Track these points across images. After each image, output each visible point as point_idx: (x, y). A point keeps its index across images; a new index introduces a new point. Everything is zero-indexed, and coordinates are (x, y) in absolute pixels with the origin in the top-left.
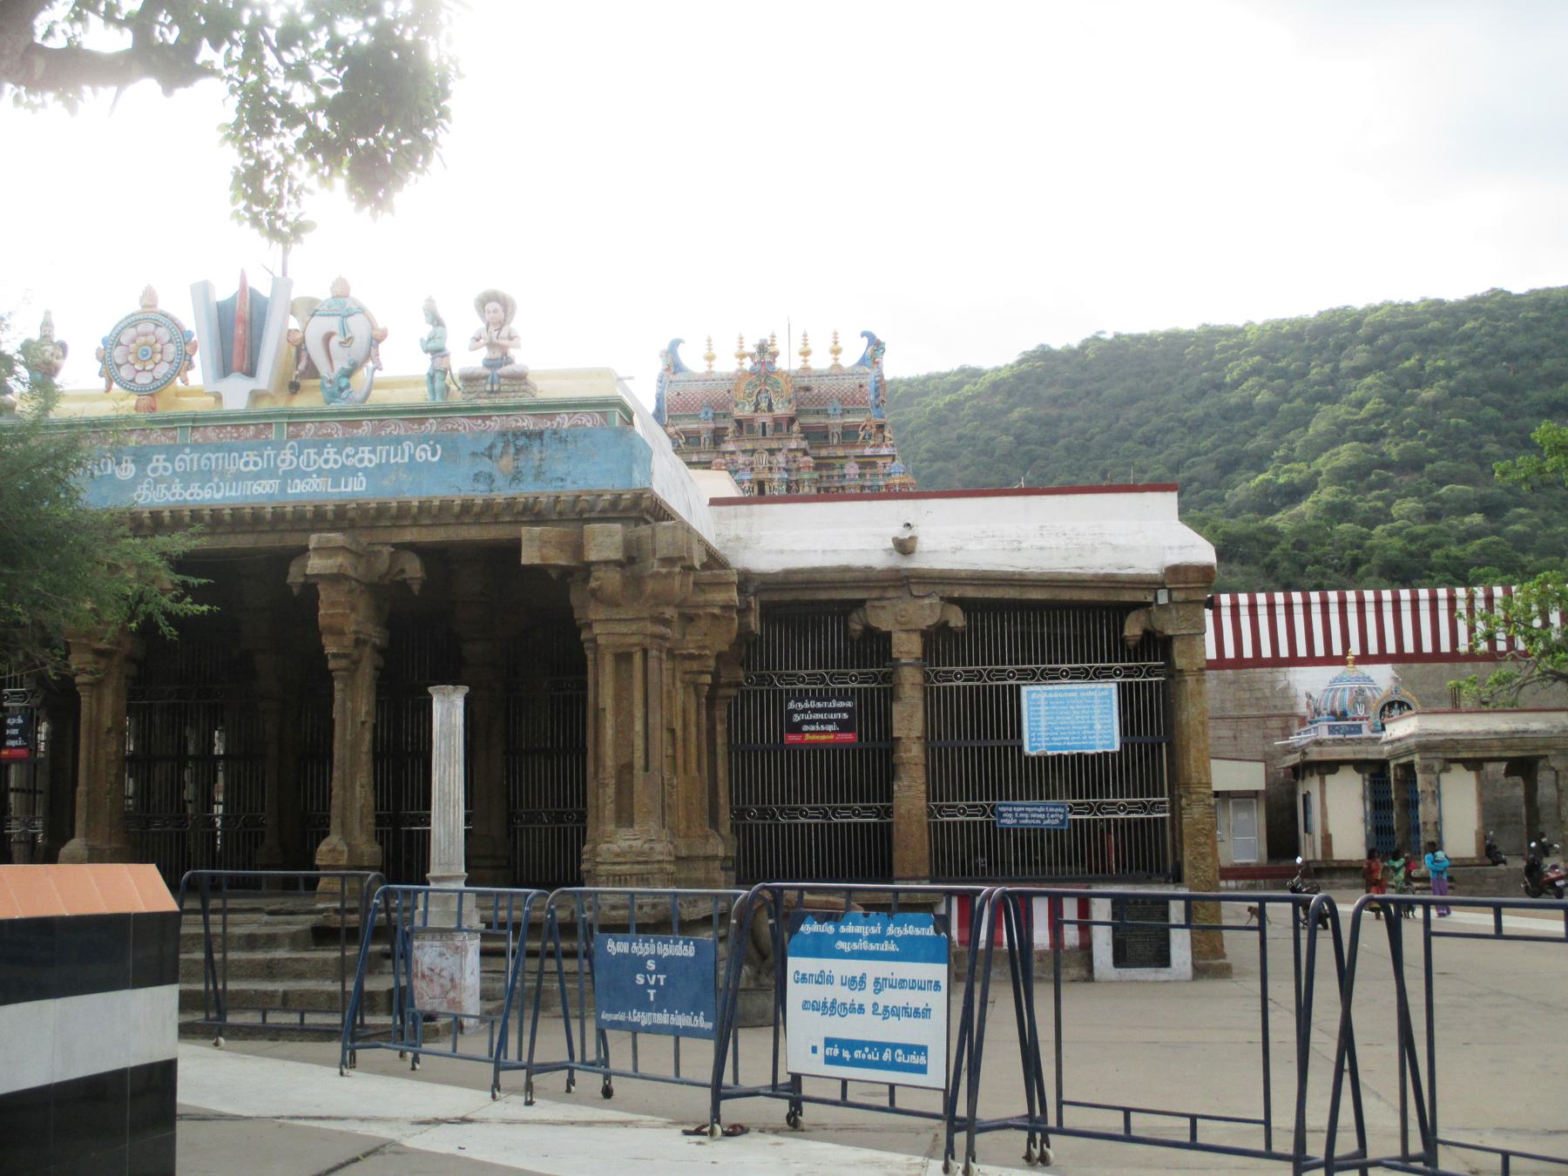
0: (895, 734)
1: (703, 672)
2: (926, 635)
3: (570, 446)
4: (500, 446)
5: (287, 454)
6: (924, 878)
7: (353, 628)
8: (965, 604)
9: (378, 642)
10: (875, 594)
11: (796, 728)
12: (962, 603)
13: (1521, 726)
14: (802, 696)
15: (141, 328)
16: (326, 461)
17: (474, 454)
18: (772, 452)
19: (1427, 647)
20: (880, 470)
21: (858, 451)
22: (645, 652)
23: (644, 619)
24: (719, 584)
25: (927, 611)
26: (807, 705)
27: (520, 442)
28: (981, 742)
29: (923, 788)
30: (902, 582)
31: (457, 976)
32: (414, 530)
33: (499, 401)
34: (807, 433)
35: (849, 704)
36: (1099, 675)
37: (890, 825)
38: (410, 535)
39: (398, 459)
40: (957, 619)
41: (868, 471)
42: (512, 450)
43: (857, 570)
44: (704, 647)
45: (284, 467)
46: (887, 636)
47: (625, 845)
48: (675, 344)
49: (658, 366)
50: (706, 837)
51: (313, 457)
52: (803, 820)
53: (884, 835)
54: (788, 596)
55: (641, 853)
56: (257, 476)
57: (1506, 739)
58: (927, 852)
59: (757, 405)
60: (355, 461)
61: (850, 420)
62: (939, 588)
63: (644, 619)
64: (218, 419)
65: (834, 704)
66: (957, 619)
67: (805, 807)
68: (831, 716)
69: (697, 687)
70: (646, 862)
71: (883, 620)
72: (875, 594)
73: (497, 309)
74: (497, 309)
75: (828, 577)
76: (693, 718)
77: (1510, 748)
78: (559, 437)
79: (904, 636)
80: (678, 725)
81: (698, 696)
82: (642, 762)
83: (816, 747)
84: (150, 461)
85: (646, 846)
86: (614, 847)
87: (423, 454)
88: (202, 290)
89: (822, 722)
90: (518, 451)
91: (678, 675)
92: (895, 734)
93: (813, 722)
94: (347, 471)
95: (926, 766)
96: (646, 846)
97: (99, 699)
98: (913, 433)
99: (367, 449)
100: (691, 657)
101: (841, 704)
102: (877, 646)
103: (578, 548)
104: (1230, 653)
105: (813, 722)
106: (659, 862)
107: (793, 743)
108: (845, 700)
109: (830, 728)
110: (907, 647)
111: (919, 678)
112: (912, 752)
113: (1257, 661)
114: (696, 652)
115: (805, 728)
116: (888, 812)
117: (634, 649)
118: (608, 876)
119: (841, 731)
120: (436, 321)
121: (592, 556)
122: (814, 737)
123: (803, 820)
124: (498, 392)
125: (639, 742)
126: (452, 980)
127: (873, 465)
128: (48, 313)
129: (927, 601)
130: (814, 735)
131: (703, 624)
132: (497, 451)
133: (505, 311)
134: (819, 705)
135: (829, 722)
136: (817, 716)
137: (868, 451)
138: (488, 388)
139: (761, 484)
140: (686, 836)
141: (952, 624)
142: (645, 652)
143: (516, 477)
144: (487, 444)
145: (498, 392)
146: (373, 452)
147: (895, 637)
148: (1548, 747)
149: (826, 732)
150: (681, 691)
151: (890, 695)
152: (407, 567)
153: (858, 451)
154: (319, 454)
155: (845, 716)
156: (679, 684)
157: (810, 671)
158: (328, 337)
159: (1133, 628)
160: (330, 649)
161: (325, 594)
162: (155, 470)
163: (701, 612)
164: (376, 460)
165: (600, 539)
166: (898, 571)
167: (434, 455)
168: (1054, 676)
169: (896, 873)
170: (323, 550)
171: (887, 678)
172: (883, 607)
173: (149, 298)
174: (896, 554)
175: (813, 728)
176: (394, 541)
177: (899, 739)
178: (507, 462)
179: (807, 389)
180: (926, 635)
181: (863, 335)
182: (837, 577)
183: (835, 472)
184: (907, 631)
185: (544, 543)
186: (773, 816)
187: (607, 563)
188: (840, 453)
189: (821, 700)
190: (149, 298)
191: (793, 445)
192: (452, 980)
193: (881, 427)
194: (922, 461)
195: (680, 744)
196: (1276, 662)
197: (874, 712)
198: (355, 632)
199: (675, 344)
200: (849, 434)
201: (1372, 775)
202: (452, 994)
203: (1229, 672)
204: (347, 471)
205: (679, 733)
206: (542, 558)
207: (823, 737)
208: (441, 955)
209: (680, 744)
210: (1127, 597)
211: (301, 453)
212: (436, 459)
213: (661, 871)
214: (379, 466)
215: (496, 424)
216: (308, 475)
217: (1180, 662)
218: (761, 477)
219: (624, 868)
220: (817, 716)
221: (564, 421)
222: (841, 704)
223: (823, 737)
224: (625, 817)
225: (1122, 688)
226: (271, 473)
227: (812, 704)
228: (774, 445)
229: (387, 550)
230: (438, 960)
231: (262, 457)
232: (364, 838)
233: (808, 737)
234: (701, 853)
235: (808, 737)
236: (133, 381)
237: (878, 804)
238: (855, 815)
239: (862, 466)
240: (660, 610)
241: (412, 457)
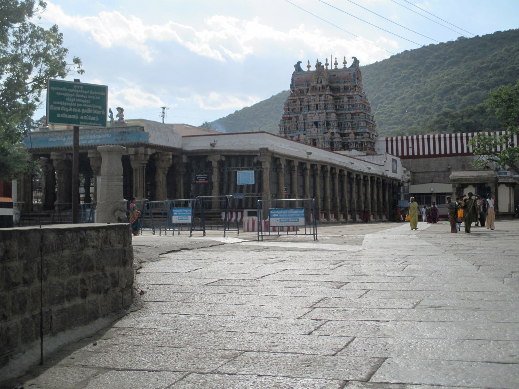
5: (88, 136)
8: (226, 156)
12: (224, 155)
13: (480, 175)
18: (320, 96)
19: (443, 152)
20: (355, 99)
21: (348, 94)
25: (218, 157)
28: (228, 182)
30: (214, 152)
34: (332, 89)
36: (252, 169)
40: (224, 159)
41: (351, 100)
46: (211, 162)
48: (299, 63)
49: (294, 70)
57: (476, 178)
59: (318, 81)
61: (346, 84)
66: (224, 159)
77: (476, 181)
78: (128, 133)
80: (161, 180)
87: (108, 136)
98: (513, 53)
100: (163, 168)
104: (460, 151)
110: (215, 164)
112: (216, 185)
113: (468, 153)
121: (129, 153)
127: (352, 98)
137: (351, 94)
139: (317, 105)
143: (122, 140)
148: (487, 180)
153: (348, 94)
159: (255, 160)
160: (93, 169)
161: (91, 160)
168: (243, 169)
170: (91, 153)
178: (121, 137)
179: (335, 75)
181: (353, 58)
183: (341, 100)
187: (132, 155)
188: (343, 94)
191: (327, 93)
193: (355, 86)
194: (516, 64)
196: (472, 154)
199: (299, 63)
200: (346, 89)
201: (478, 188)
203: (459, 157)
210: (254, 154)
215: (120, 130)
217: (263, 167)
218: (317, 103)
221: (130, 129)
225: (255, 172)
226: (85, 139)
228: (321, 93)
235: (200, 182)
239: (349, 98)
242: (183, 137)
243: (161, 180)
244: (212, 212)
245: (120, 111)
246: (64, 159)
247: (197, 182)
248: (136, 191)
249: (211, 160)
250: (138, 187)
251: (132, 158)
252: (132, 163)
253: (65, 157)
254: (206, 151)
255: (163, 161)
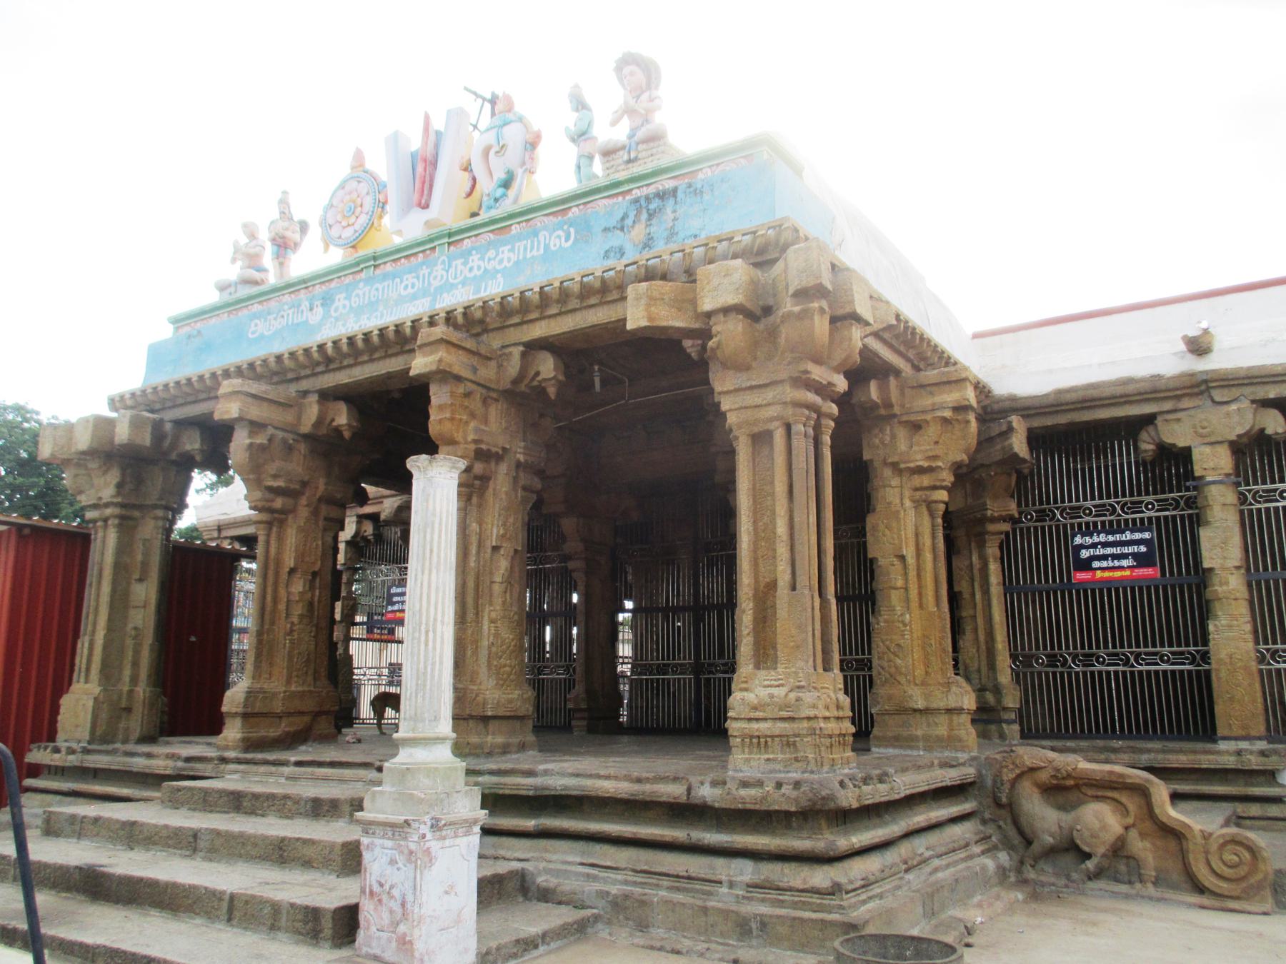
0: (1206, 565)
1: (935, 488)
2: (1239, 449)
3: (706, 197)
4: (632, 214)
6: (1260, 738)
7: (471, 437)
9: (521, 458)
10: (1168, 406)
11: (1085, 565)
14: (1088, 530)
15: (348, 188)
16: (471, 269)
17: (606, 230)
22: (788, 427)
23: (781, 382)
24: (949, 382)
25: (1238, 418)
26: (1096, 539)
27: (652, 206)
29: (1248, 627)
30: (1199, 388)
31: (410, 898)
32: (544, 323)
33: (637, 169)
35: (1147, 535)
37: (1208, 673)
38: (539, 331)
39: (535, 253)
42: (644, 216)
43: (1143, 380)
44: (935, 457)
45: (436, 283)
47: (763, 693)
50: (948, 685)
51: (460, 267)
52: (1099, 667)
53: (1203, 682)
54: (1062, 419)
55: (786, 706)
56: (414, 297)
58: (1260, 706)
60: (494, 264)
62: (1247, 390)
63: (781, 382)
64: (392, 253)
65: (1128, 536)
67: (1102, 652)
68: (1126, 550)
69: (930, 504)
70: (792, 719)
71: (1177, 434)
72: (1168, 406)
73: (639, 74)
74: (639, 74)
75: (1108, 392)
76: (927, 541)
79: (1207, 450)
80: (909, 552)
81: (932, 516)
82: (787, 577)
83: (1112, 589)
84: (333, 301)
85: (792, 695)
86: (751, 697)
88: (395, 140)
89: (1115, 557)
90: (651, 216)
91: (907, 493)
92: (1206, 565)
93: (1104, 557)
94: (488, 274)
95: (1251, 602)
96: (792, 695)
97: (281, 539)
99: (506, 249)
100: (920, 471)
101: (1137, 536)
102: (1174, 466)
103: (688, 302)
105: (1104, 557)
106: (809, 718)
107: (1082, 582)
108: (1141, 531)
109: (1125, 563)
110: (1213, 462)
111: (1231, 497)
114: (926, 464)
115: (1096, 564)
116: (1205, 657)
117: (772, 426)
118: (743, 737)
119: (1139, 566)
120: (580, 105)
121: (707, 305)
122: (1107, 574)
123: (1099, 667)
124: (636, 159)
125: (782, 551)
126: (403, 905)
128: (285, 193)
129: (1234, 407)
130: (1102, 572)
131: (933, 431)
132: (629, 222)
133: (649, 78)
134: (1111, 538)
135: (1124, 556)
136: (1109, 551)
138: (626, 157)
140: (924, 684)
141: (1269, 431)
142: (788, 427)
144: (621, 215)
145: (636, 159)
146: (512, 250)
147: (1196, 455)
149: (1121, 568)
150: (912, 513)
151: (1197, 521)
152: (541, 369)
154: (465, 264)
155: (1143, 549)
156: (908, 503)
157: (1097, 502)
158: (486, 152)
161: (438, 396)
162: (336, 310)
163: (928, 417)
164: (514, 258)
165: (715, 282)
166: (1192, 375)
167: (567, 240)
169: (1221, 731)
171: (1190, 503)
172: (1178, 420)
173: (359, 160)
174: (1189, 356)
175: (1104, 564)
176: (526, 339)
177: (1211, 570)
178: (639, 232)
180: (1239, 449)
182: (1119, 390)
184: (1212, 444)
185: (652, 300)
186: (1064, 663)
187: (726, 310)
189: (1113, 533)
190: (359, 160)
192: (403, 905)
195: (912, 574)
197: (1178, 542)
198: (475, 441)
202: (402, 928)
204: (488, 274)
205: (911, 560)
206: (650, 319)
207: (1118, 574)
208: (393, 862)
209: (912, 574)
211: (450, 266)
212: (570, 242)
213: (812, 732)
214: (517, 263)
216: (453, 286)
219: (763, 726)
220: (1109, 551)
222: (1137, 536)
223: (1118, 574)
224: (765, 655)
227: (1102, 538)
229: (517, 352)
230: (389, 870)
231: (418, 278)
232: (492, 682)
233: (1099, 574)
234: (942, 705)
235: (1099, 574)
236: (340, 237)
237: (1192, 648)
238: (1166, 661)
240: (802, 367)
241: (547, 247)
242: (976, 336)
243: (909, 552)
244: (1230, 762)
245: (640, 77)
246: (306, 427)
247: (1081, 576)
248: (764, 618)
249: (1181, 443)
250: (784, 578)
251: (730, 333)
252: (722, 382)
253: (312, 411)
254: (1156, 390)
255: (916, 427)
